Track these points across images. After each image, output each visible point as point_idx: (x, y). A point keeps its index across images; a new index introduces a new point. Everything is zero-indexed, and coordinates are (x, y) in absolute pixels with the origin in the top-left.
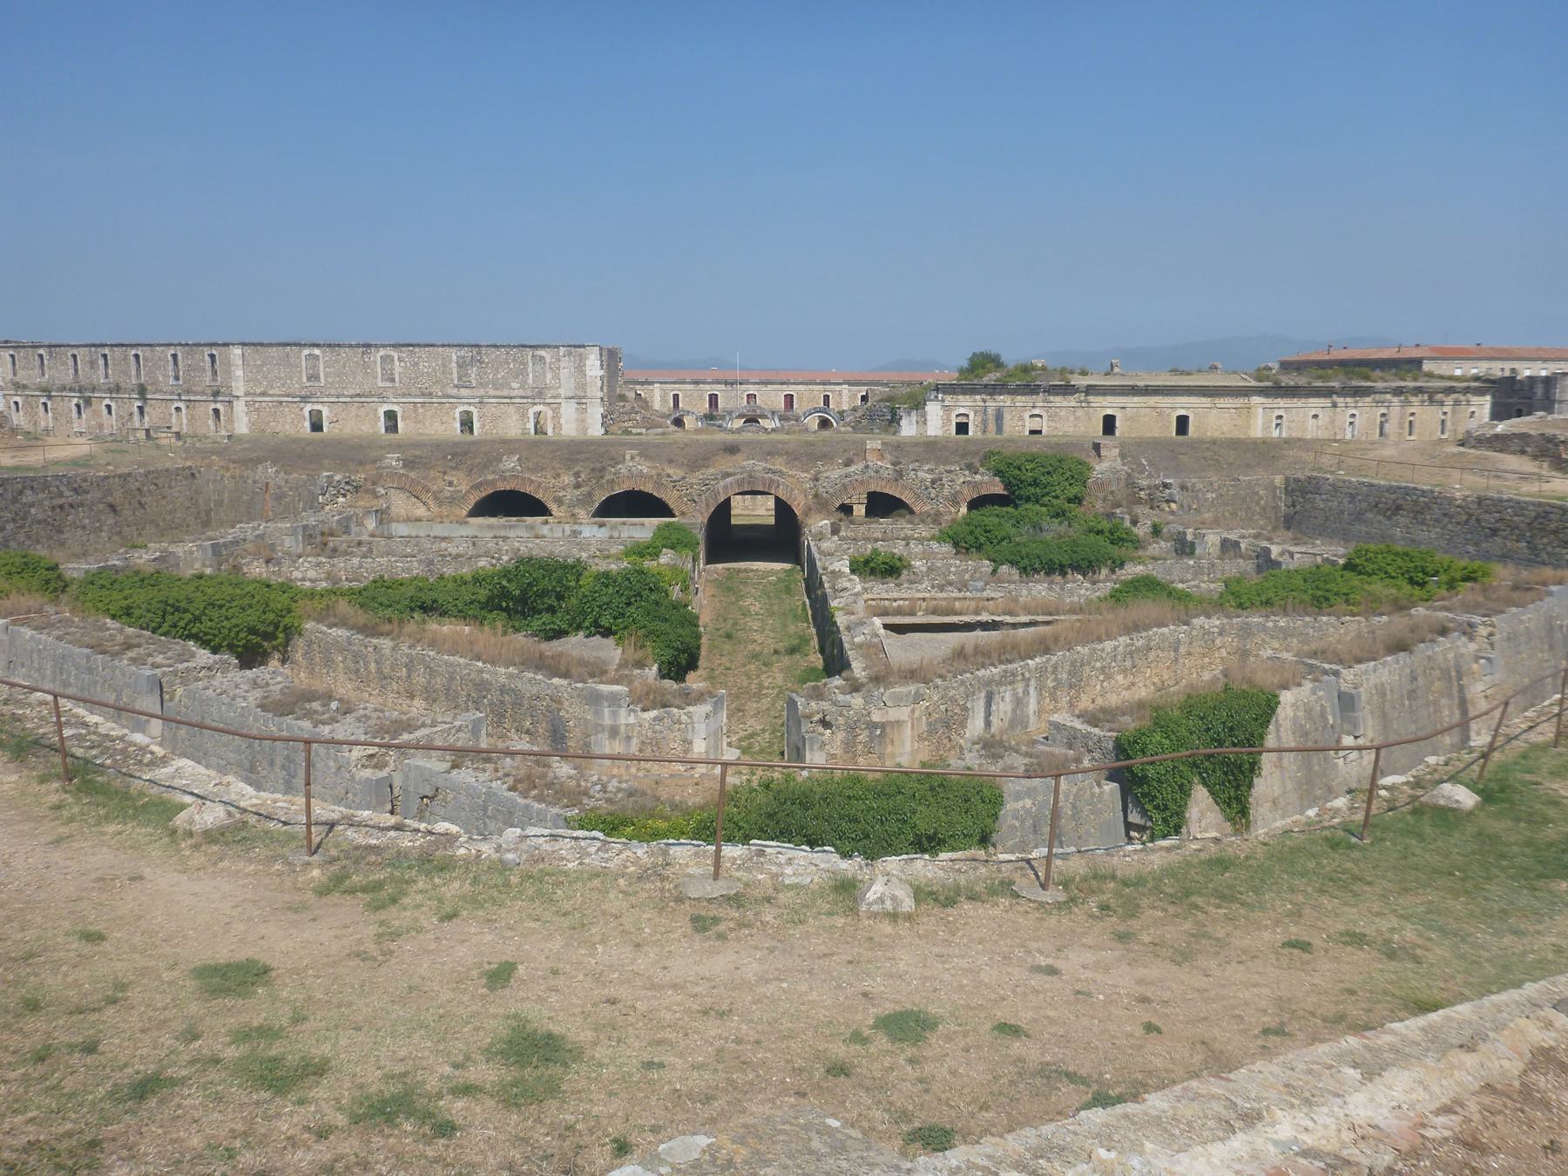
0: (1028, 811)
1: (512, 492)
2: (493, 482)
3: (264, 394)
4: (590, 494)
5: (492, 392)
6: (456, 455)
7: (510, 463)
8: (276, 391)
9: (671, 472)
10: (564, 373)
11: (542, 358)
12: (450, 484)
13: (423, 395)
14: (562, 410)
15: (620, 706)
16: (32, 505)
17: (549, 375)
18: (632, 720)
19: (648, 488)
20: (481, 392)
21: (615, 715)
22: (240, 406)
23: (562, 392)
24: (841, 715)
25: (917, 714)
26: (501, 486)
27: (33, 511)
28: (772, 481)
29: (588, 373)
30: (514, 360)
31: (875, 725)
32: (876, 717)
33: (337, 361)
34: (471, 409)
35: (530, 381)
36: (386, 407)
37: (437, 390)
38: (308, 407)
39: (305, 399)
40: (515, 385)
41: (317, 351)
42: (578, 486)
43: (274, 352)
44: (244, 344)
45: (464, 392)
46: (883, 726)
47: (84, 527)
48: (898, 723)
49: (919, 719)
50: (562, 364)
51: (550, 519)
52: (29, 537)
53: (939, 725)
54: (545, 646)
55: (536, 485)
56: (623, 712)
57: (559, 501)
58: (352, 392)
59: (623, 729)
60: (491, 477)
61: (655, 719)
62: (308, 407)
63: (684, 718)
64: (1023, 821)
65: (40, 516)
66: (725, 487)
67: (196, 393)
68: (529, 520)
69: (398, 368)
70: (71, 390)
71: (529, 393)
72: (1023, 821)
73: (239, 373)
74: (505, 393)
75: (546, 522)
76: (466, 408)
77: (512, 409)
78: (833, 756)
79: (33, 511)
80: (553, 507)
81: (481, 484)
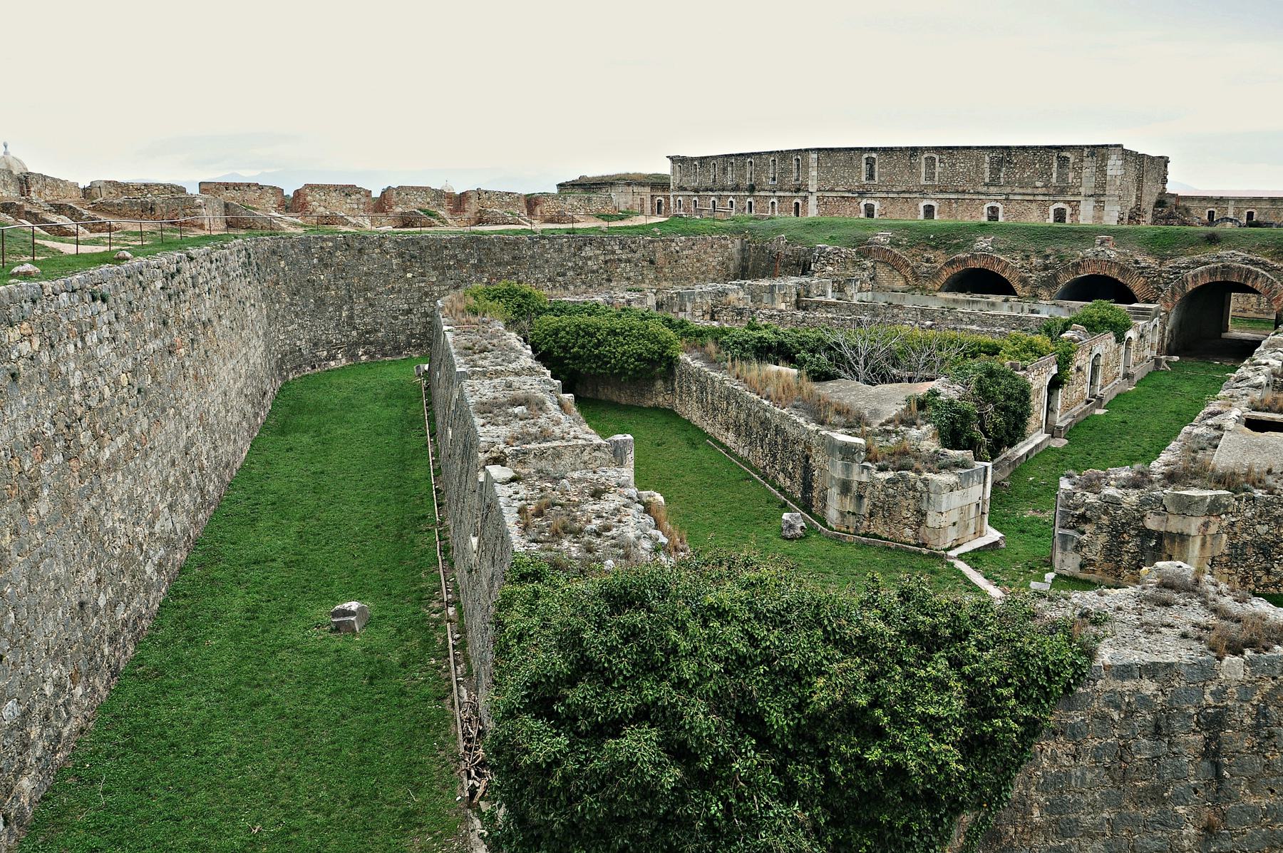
0: (1145, 701)
1: (981, 270)
2: (965, 260)
3: (832, 190)
4: (1055, 277)
5: (1017, 190)
6: (946, 239)
7: (983, 243)
8: (841, 188)
9: (1140, 259)
10: (1086, 173)
11: (1066, 159)
12: (928, 260)
13: (957, 192)
14: (1081, 208)
15: (853, 461)
16: (590, 258)
17: (1071, 175)
18: (864, 478)
19: (1114, 273)
20: (1008, 190)
21: (847, 468)
22: (812, 201)
23: (1082, 190)
24: (1106, 512)
25: (1213, 529)
26: (974, 264)
27: (589, 263)
28: (1249, 271)
29: (1109, 173)
30: (1040, 161)
31: (1148, 534)
32: (1152, 523)
33: (889, 163)
34: (998, 205)
35: (1054, 180)
36: (926, 203)
37: (969, 187)
38: (864, 202)
39: (862, 195)
40: (1038, 184)
41: (874, 155)
42: (1046, 268)
43: (841, 156)
44: (819, 150)
45: (992, 189)
46: (1160, 536)
47: (628, 279)
48: (1183, 538)
49: (1214, 537)
50: (1085, 164)
51: (1012, 298)
52: (584, 283)
53: (1250, 551)
54: (815, 386)
55: (1010, 265)
56: (856, 468)
57: (1024, 282)
58: (899, 189)
59: (855, 485)
60: (961, 255)
61: (888, 481)
62: (864, 202)
63: (919, 485)
64: (1130, 714)
65: (595, 268)
66: (1195, 276)
67: (785, 191)
68: (993, 298)
69: (938, 169)
70: (712, 190)
71: (1051, 191)
72: (1130, 714)
73: (815, 173)
74: (1029, 191)
75: (1006, 301)
76: (993, 204)
77: (1034, 206)
78: (1091, 562)
79: (589, 263)
80: (1017, 286)
81: (953, 262)
